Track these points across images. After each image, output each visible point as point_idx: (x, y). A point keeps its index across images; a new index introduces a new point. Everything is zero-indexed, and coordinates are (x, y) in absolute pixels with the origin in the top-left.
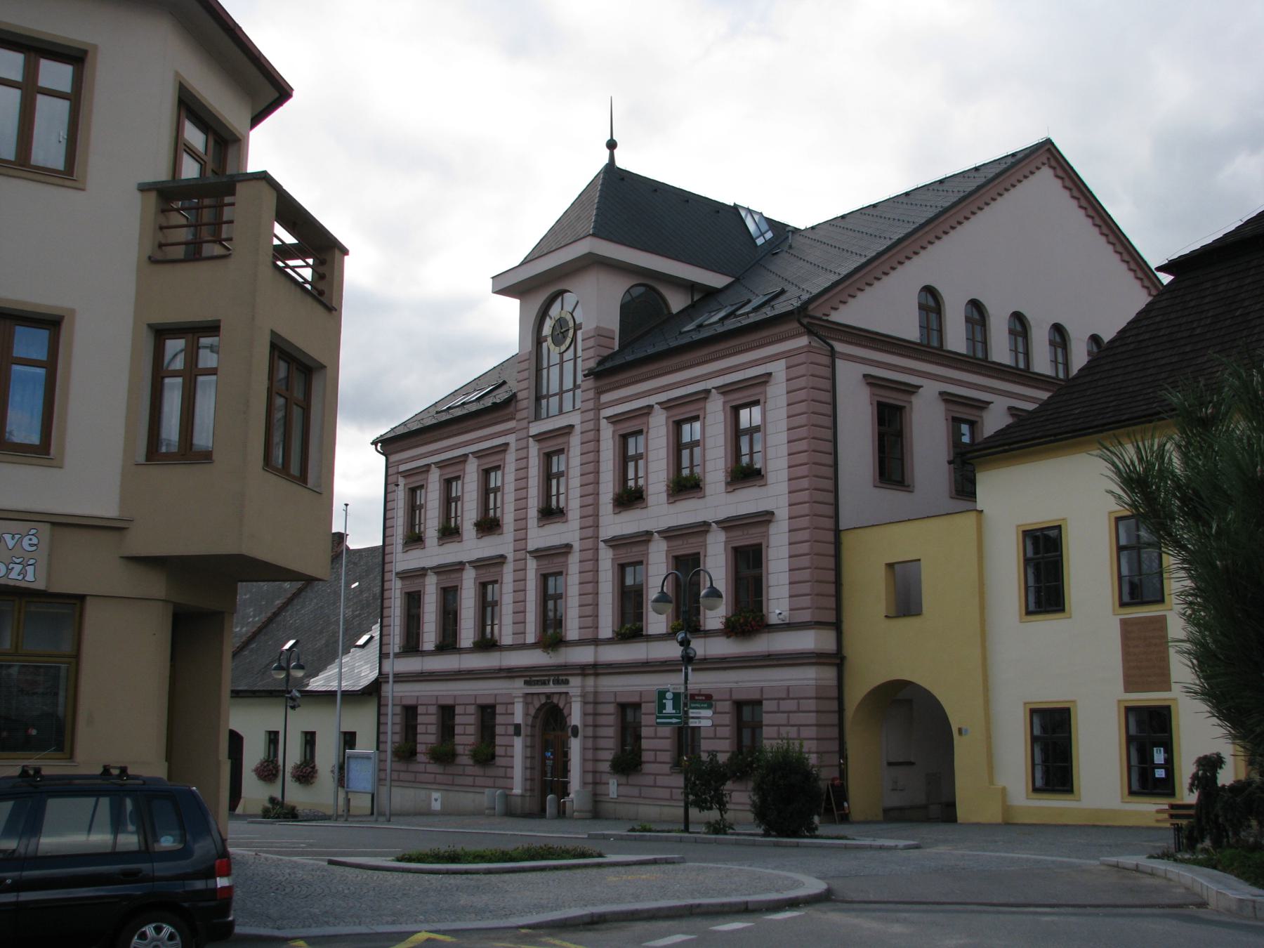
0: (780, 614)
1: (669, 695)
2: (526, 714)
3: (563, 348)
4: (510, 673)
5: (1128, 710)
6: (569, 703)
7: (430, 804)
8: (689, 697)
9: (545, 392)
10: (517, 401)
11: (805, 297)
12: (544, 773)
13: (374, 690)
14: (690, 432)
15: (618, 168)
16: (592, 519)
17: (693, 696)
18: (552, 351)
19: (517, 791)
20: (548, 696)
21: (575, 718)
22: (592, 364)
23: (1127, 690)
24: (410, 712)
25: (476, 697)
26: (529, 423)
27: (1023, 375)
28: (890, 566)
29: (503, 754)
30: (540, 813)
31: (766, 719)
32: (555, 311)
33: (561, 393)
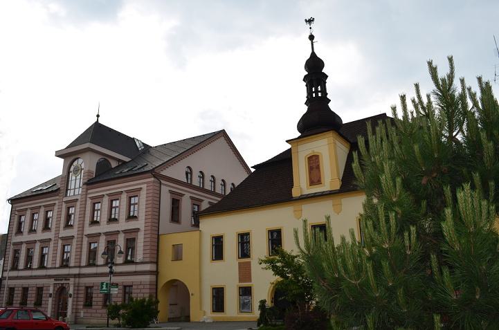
2: (54, 290)
4: (50, 277)
5: (240, 288)
6: (69, 286)
11: (154, 167)
12: (58, 309)
14: (115, 204)
16: (82, 228)
18: (72, 177)
20: (62, 284)
21: (71, 291)
22: (86, 181)
24: (12, 290)
27: (213, 193)
28: (173, 245)
31: (94, 292)
32: (75, 163)
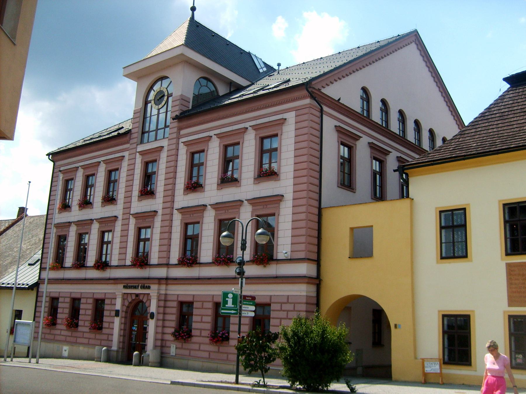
0: (286, 253)
1: (230, 296)
2: (123, 305)
3: (160, 106)
4: (116, 281)
5: (510, 317)
7: (62, 352)
8: (242, 298)
9: (147, 129)
10: (131, 134)
12: (130, 339)
13: (36, 285)
15: (196, 21)
17: (245, 297)
18: (153, 110)
19: (115, 348)
20: (137, 295)
21: (153, 308)
22: (178, 113)
23: (510, 305)
24: (54, 301)
25: (94, 294)
26: (137, 145)
28: (352, 229)
29: (107, 326)
30: (127, 361)
32: (157, 88)
33: (157, 129)
